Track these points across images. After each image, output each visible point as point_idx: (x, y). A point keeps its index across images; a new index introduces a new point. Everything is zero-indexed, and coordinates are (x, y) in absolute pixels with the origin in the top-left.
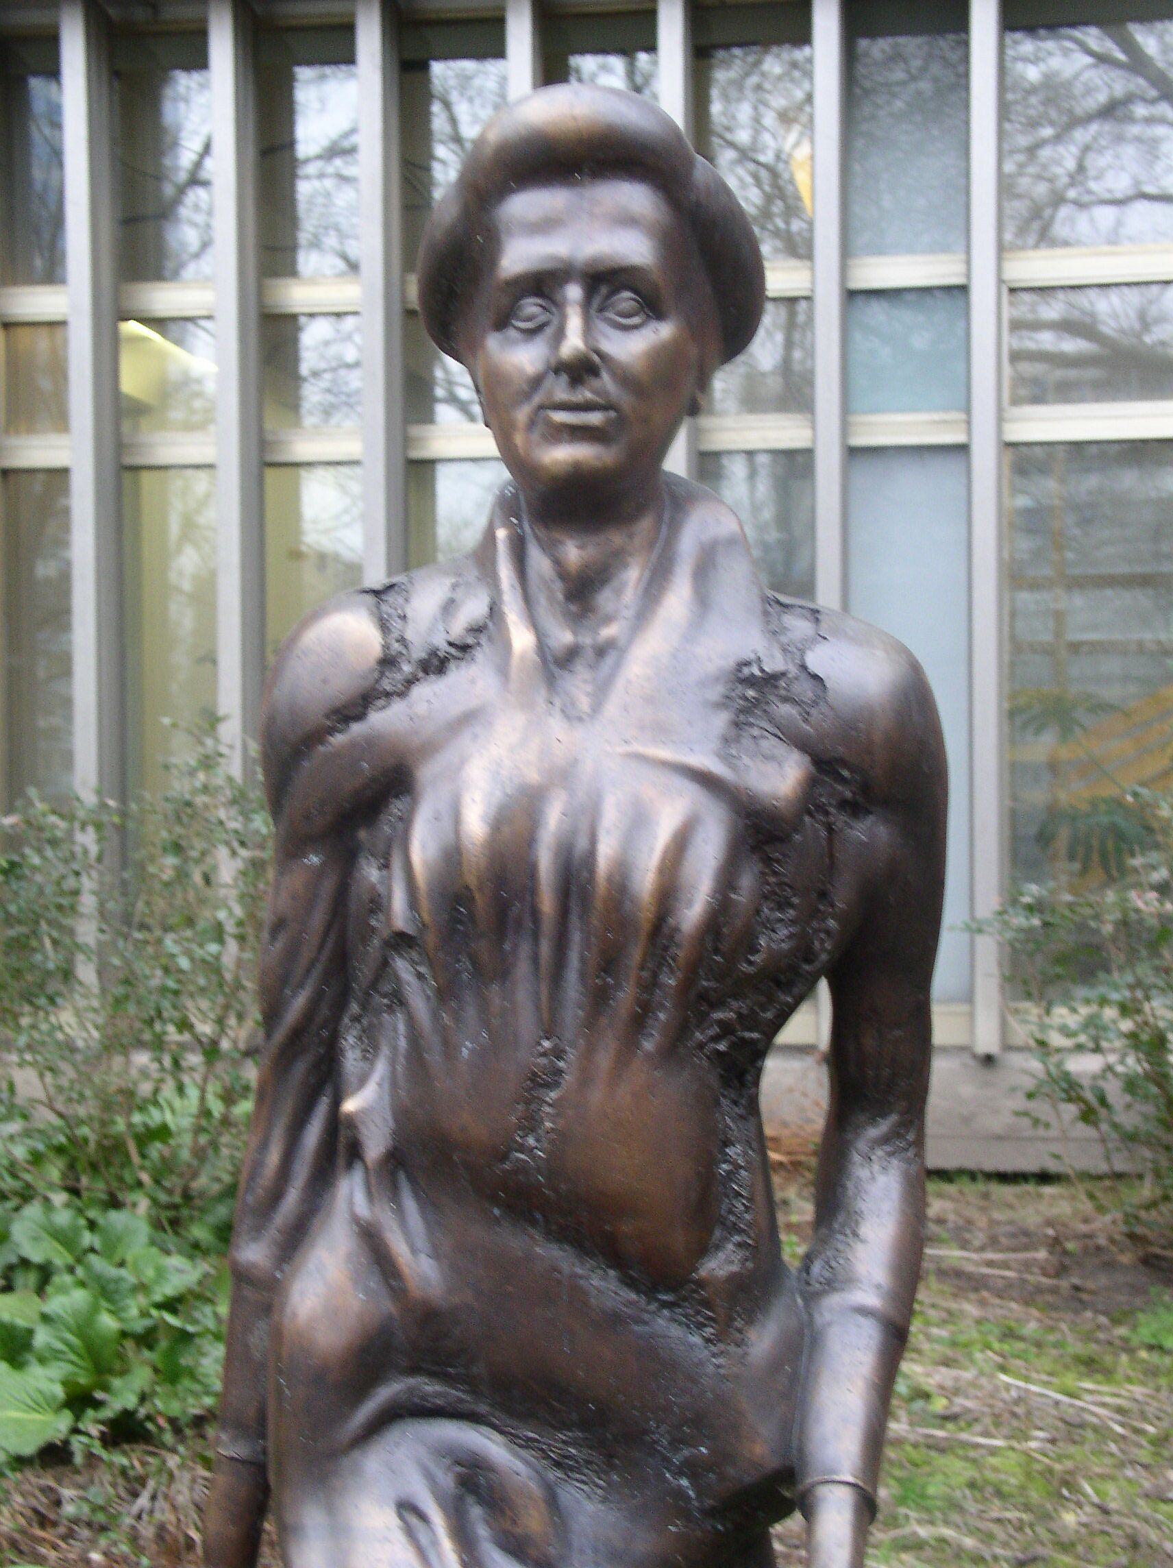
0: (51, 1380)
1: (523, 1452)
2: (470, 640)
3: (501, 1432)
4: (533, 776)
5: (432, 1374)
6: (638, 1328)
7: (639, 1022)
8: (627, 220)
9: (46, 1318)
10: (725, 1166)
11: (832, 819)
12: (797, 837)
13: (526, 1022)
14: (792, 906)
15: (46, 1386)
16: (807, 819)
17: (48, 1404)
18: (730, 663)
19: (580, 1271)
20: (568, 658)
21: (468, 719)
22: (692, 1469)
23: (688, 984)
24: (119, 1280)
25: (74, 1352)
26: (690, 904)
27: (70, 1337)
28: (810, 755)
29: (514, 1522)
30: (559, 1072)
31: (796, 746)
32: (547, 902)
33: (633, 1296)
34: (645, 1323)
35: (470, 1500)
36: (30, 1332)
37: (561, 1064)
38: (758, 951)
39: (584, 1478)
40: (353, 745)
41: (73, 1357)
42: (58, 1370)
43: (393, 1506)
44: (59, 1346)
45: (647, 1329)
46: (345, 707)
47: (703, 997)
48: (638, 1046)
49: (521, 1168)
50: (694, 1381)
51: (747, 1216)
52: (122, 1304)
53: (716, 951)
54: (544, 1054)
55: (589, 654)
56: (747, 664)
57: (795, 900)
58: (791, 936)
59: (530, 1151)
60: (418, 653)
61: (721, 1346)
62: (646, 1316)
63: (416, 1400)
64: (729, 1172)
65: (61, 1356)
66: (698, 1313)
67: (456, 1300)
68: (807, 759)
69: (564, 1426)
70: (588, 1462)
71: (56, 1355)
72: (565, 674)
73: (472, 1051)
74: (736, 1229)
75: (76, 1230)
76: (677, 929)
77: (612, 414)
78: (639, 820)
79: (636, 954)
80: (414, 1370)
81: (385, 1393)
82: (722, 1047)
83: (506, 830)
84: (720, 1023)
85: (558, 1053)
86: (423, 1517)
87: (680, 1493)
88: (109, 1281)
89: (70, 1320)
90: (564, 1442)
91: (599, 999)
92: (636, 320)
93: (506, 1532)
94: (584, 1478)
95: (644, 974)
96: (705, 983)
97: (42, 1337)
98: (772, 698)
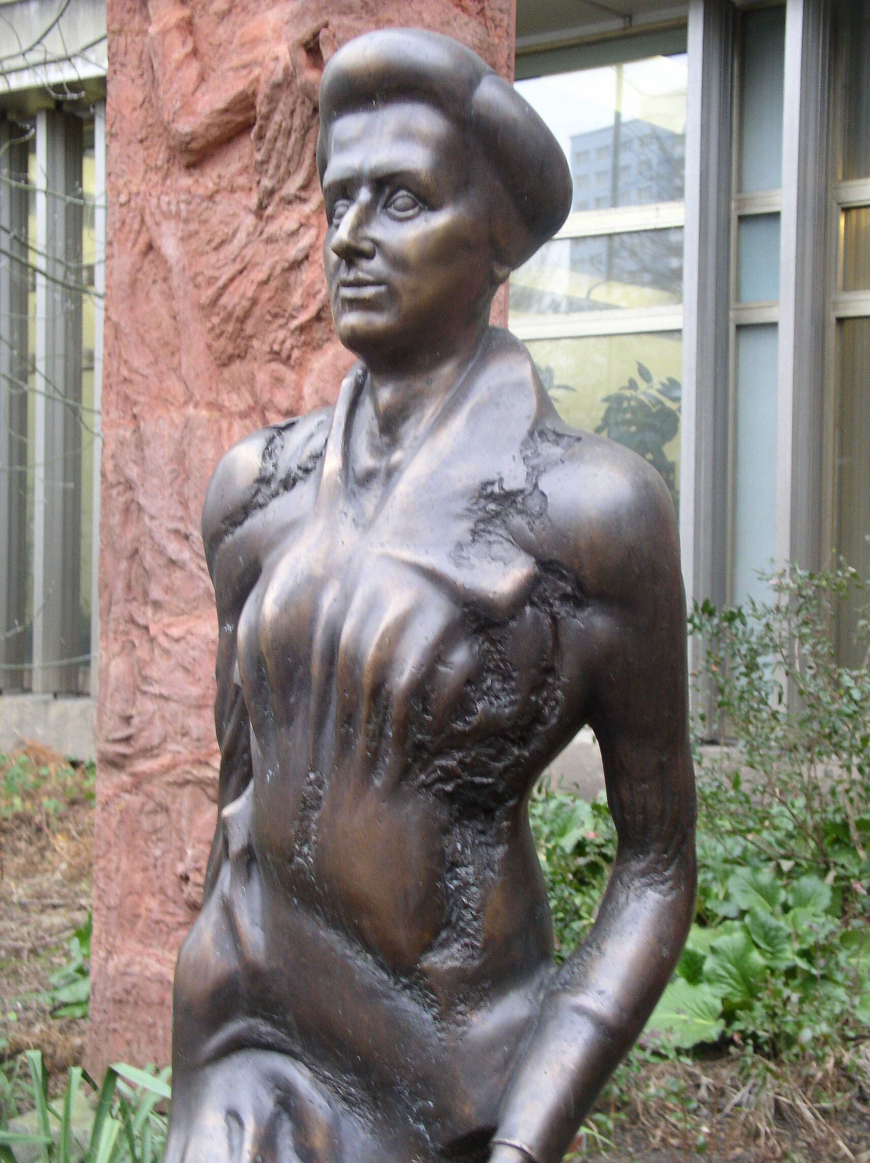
0: (715, 996)
1: (323, 1086)
2: (310, 466)
3: (310, 1069)
4: (319, 571)
5: (265, 1018)
6: (386, 1002)
7: (371, 764)
8: (405, 135)
9: (713, 950)
10: (455, 882)
11: (555, 609)
12: (513, 624)
13: (300, 758)
14: (513, 679)
15: (709, 999)
16: (528, 609)
17: (710, 1012)
18: (476, 482)
19: (348, 952)
20: (369, 476)
21: (288, 529)
22: (424, 1116)
23: (402, 736)
24: (778, 929)
25: (732, 978)
26: (402, 673)
27: (729, 966)
28: (535, 557)
29: (306, 1138)
30: (319, 798)
31: (522, 548)
32: (316, 667)
33: (385, 977)
34: (392, 999)
35: (285, 1117)
36: (704, 958)
37: (321, 792)
38: (475, 714)
39: (361, 1112)
40: (235, 543)
41: (731, 981)
42: (723, 989)
43: (224, 1113)
44: (722, 972)
45: (393, 1004)
46: (232, 515)
47: (420, 747)
48: (370, 782)
49: (300, 870)
50: (424, 1050)
51: (475, 924)
52: (779, 947)
53: (425, 711)
54: (310, 784)
55: (382, 475)
56: (492, 483)
57: (515, 674)
58: (512, 703)
59: (305, 857)
60: (281, 475)
61: (444, 1024)
62: (393, 994)
63: (255, 1037)
64: (458, 888)
65: (724, 980)
66: (426, 996)
67: (274, 965)
68: (533, 560)
69: (346, 1071)
70: (363, 1101)
71: (719, 979)
72: (363, 491)
73: (271, 777)
74: (463, 932)
75: (775, 889)
76: (389, 693)
77: (382, 289)
78: (373, 606)
79: (363, 711)
80: (253, 1014)
81: (234, 1028)
82: (449, 788)
83: (293, 611)
84: (442, 768)
85: (319, 783)
86: (241, 1124)
87: (418, 1135)
88: (770, 929)
89: (731, 956)
90: (347, 1082)
91: (345, 743)
92: (410, 213)
93: (302, 1146)
94: (361, 1112)
95: (371, 727)
96: (419, 736)
97: (709, 964)
98: (512, 510)
